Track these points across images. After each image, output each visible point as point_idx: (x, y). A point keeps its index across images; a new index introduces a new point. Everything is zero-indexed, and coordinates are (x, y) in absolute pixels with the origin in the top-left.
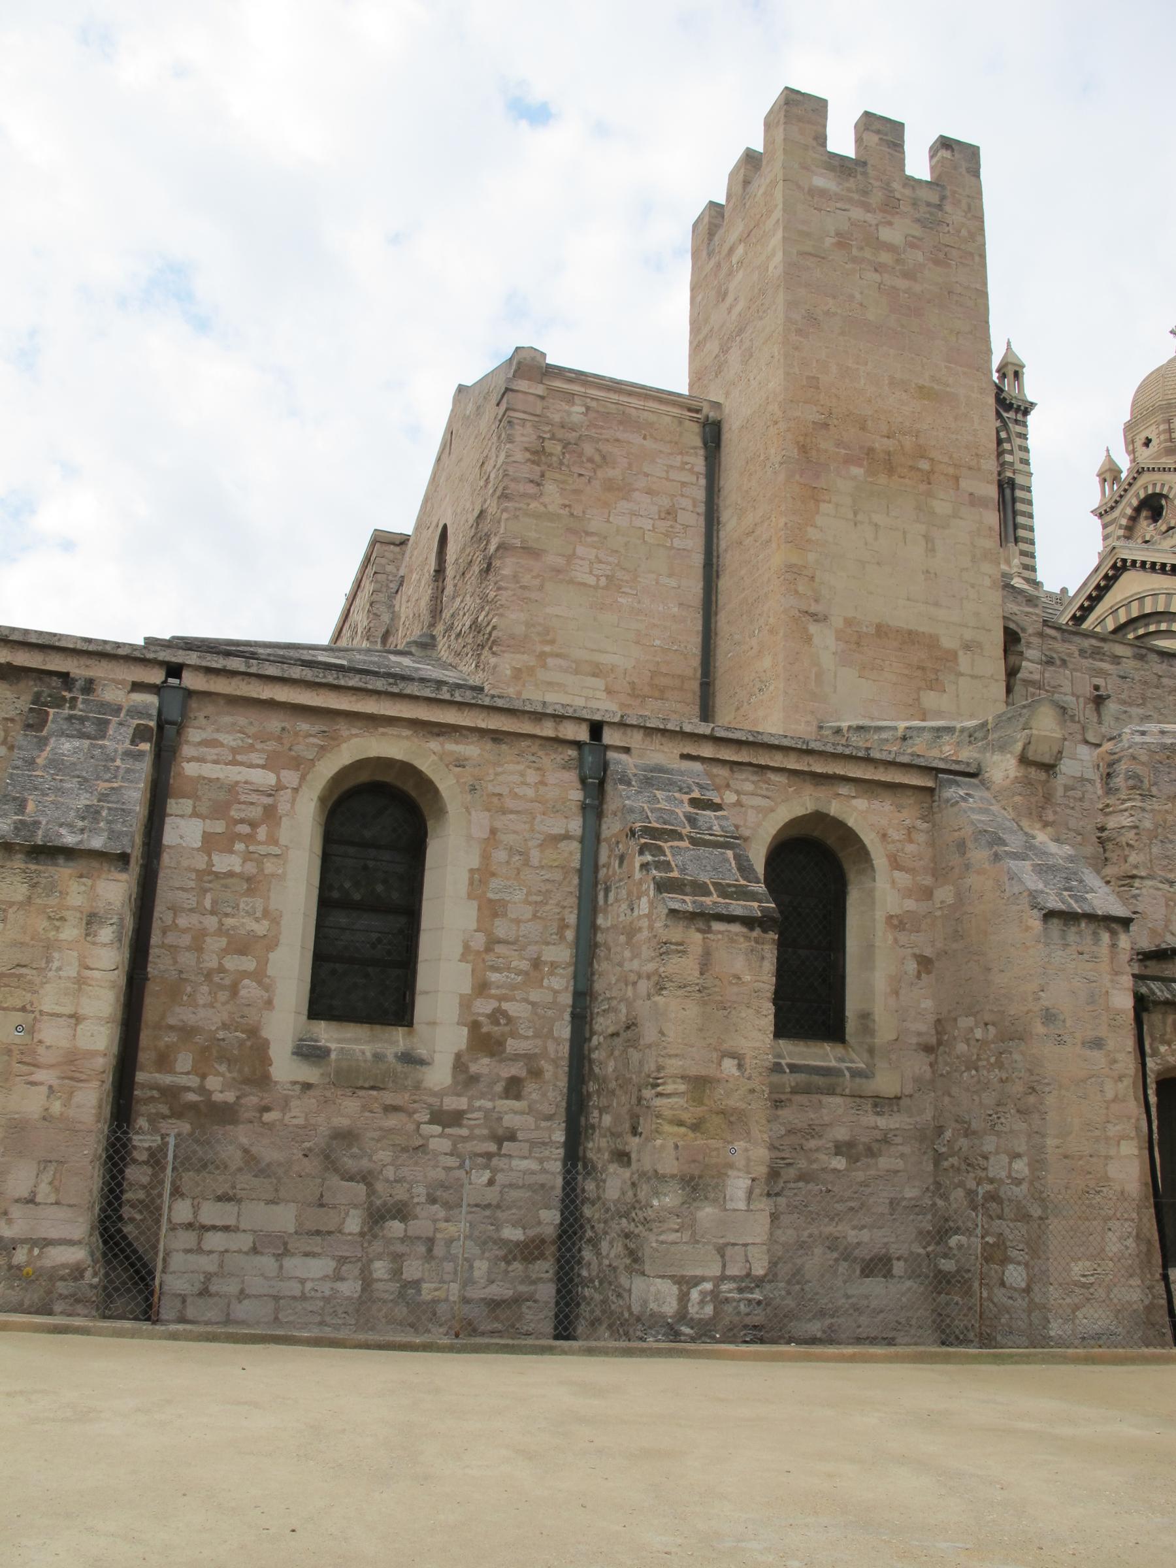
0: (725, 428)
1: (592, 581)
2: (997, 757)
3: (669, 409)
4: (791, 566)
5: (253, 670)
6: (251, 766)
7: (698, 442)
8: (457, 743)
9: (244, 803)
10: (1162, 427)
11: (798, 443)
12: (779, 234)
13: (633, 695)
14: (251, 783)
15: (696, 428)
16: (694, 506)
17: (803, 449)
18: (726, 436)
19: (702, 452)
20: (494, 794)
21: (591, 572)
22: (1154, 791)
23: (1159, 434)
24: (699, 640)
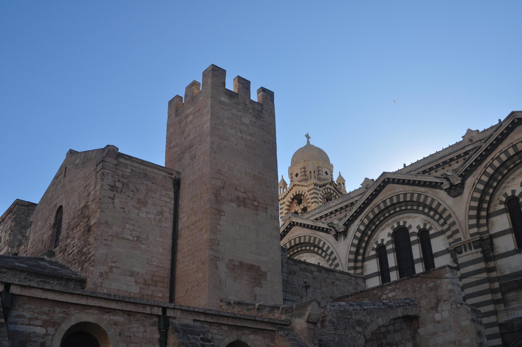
0: (182, 182)
1: (131, 238)
2: (297, 320)
3: (162, 173)
4: (211, 239)
5: (41, 286)
6: (36, 326)
7: (172, 187)
8: (115, 316)
9: (33, 341)
10: (302, 170)
11: (214, 193)
12: (209, 116)
13: (145, 284)
14: (36, 333)
15: (171, 181)
16: (170, 211)
17: (216, 196)
18: (182, 185)
19: (173, 190)
20: (128, 336)
21: (131, 235)
22: (339, 328)
23: (301, 172)
24: (170, 263)
